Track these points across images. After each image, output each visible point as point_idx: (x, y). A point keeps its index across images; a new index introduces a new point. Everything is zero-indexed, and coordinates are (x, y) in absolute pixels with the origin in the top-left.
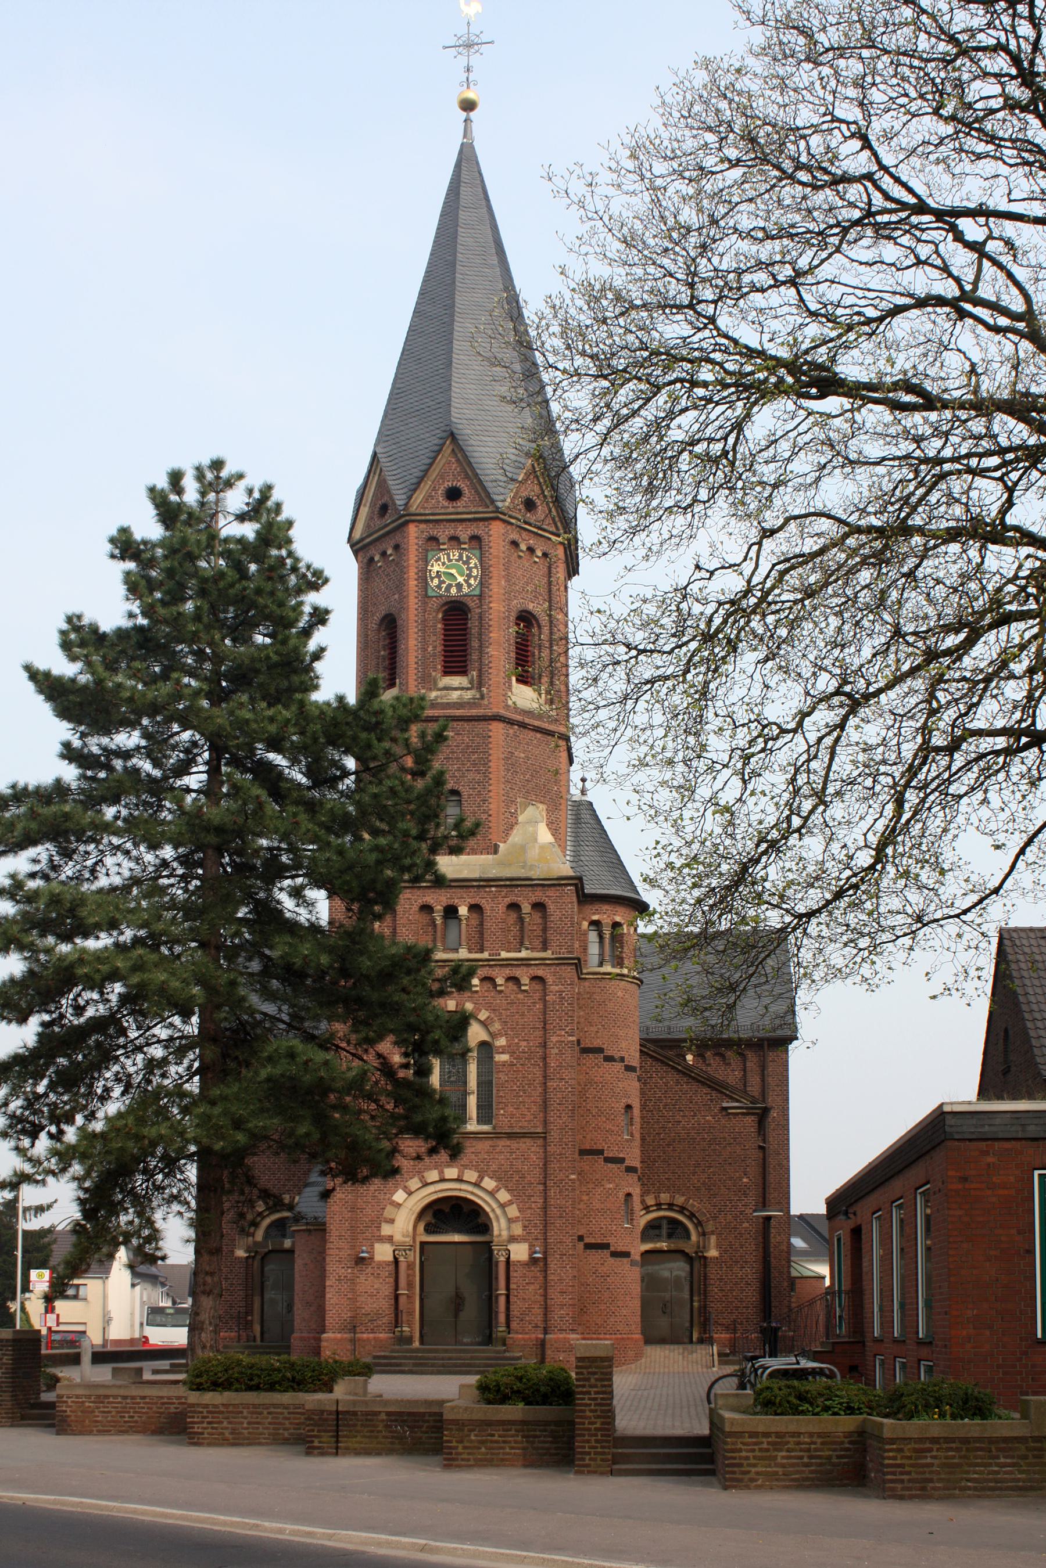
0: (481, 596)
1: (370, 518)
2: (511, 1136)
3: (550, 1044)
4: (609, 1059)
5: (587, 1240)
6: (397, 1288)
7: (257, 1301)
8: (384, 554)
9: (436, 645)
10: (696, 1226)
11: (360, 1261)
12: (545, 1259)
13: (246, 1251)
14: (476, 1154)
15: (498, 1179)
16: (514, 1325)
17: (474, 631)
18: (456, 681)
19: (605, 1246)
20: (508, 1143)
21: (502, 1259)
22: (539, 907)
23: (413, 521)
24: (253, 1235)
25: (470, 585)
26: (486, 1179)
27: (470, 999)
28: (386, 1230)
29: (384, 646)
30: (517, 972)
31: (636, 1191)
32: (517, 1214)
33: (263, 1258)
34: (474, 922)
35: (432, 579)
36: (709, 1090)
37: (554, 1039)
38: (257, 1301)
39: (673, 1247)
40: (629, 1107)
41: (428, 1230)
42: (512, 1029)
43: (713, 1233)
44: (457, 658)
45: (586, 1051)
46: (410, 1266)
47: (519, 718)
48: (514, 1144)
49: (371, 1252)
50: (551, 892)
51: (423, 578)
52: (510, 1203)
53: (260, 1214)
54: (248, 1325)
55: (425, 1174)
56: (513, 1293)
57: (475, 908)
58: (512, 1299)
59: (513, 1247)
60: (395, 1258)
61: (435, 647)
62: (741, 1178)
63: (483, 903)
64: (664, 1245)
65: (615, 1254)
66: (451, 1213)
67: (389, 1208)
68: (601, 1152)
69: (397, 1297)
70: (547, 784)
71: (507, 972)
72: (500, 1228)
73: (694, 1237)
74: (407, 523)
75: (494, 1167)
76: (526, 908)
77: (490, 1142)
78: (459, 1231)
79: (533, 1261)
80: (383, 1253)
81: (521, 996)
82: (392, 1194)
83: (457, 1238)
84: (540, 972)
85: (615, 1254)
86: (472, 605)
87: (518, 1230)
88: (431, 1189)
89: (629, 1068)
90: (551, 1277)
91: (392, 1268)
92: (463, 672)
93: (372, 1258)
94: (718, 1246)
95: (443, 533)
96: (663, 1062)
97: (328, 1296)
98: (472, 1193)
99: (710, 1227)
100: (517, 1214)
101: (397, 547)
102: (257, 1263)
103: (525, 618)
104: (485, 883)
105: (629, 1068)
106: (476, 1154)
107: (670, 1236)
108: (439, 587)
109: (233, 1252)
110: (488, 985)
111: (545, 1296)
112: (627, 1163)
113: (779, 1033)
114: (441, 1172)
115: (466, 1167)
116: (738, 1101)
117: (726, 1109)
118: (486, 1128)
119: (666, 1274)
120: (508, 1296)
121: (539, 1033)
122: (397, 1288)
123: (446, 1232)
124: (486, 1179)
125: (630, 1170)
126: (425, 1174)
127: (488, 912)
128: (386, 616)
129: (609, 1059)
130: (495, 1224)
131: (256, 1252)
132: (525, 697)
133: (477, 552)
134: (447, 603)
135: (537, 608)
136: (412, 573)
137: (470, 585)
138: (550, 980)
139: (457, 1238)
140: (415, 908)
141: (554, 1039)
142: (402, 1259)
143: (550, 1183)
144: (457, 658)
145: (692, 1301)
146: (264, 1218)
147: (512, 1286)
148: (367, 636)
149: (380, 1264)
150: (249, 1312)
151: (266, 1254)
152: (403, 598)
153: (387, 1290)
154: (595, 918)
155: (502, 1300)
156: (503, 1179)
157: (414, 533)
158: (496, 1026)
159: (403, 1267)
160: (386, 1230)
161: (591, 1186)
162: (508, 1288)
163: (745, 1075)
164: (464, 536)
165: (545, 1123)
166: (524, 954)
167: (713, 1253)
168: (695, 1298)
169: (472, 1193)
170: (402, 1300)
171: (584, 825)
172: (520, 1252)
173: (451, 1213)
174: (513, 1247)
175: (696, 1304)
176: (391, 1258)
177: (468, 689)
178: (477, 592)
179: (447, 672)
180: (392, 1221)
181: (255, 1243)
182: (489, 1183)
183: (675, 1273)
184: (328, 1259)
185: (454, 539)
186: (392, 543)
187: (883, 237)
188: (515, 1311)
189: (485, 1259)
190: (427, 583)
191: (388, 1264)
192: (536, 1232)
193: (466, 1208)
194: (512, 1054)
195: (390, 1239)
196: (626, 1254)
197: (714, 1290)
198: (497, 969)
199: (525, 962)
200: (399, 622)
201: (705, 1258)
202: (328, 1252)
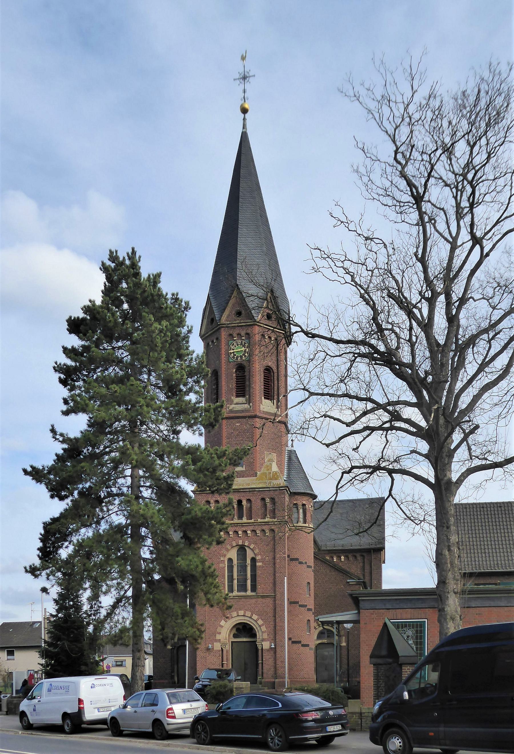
1: (207, 325)
2: (263, 597)
4: (301, 563)
5: (293, 640)
7: (176, 667)
8: (213, 342)
9: (233, 385)
12: (275, 648)
15: (258, 615)
16: (264, 675)
18: (241, 400)
19: (299, 642)
20: (262, 600)
23: (223, 327)
25: (245, 356)
28: (218, 637)
30: (264, 528)
31: (312, 618)
36: (342, 574)
37: (278, 556)
38: (176, 667)
39: (329, 642)
40: (309, 583)
41: (235, 636)
44: (242, 389)
45: (292, 560)
46: (227, 651)
47: (264, 416)
48: (264, 600)
49: (213, 647)
52: (263, 625)
54: (172, 677)
56: (264, 662)
61: (232, 385)
63: (251, 498)
64: (325, 641)
65: (304, 646)
68: (298, 603)
70: (278, 444)
72: (259, 635)
74: (219, 329)
75: (257, 610)
77: (255, 600)
78: (245, 637)
80: (217, 646)
83: (245, 640)
85: (304, 646)
87: (265, 636)
88: (234, 619)
89: (309, 567)
92: (244, 396)
96: (325, 562)
101: (217, 339)
102: (175, 651)
104: (252, 490)
105: (309, 567)
107: (328, 637)
110: (253, 533)
111: (275, 663)
112: (308, 607)
113: (378, 546)
114: (238, 613)
115: (246, 610)
116: (353, 579)
117: (349, 582)
118: (254, 594)
119: (326, 653)
120: (262, 663)
121: (272, 553)
123: (241, 637)
125: (309, 610)
127: (253, 502)
128: (214, 370)
129: (301, 563)
130: (257, 634)
131: (175, 647)
132: (267, 406)
135: (272, 364)
136: (223, 351)
137: (245, 356)
139: (245, 640)
142: (224, 649)
143: (277, 616)
144: (242, 389)
147: (264, 659)
150: (173, 671)
152: (220, 362)
154: (295, 502)
156: (260, 615)
158: (257, 551)
159: (225, 652)
160: (218, 637)
161: (294, 617)
163: (364, 565)
164: (243, 333)
165: (275, 591)
166: (267, 520)
171: (293, 461)
172: (266, 645)
173: (244, 629)
177: (245, 404)
179: (237, 396)
181: (175, 643)
182: (255, 617)
183: (330, 653)
186: (215, 337)
187: (278, 321)
188: (265, 671)
189: (254, 650)
190: (229, 356)
191: (219, 651)
192: (272, 637)
193: (248, 627)
194: (263, 562)
196: (307, 645)
199: (267, 523)
200: (219, 374)
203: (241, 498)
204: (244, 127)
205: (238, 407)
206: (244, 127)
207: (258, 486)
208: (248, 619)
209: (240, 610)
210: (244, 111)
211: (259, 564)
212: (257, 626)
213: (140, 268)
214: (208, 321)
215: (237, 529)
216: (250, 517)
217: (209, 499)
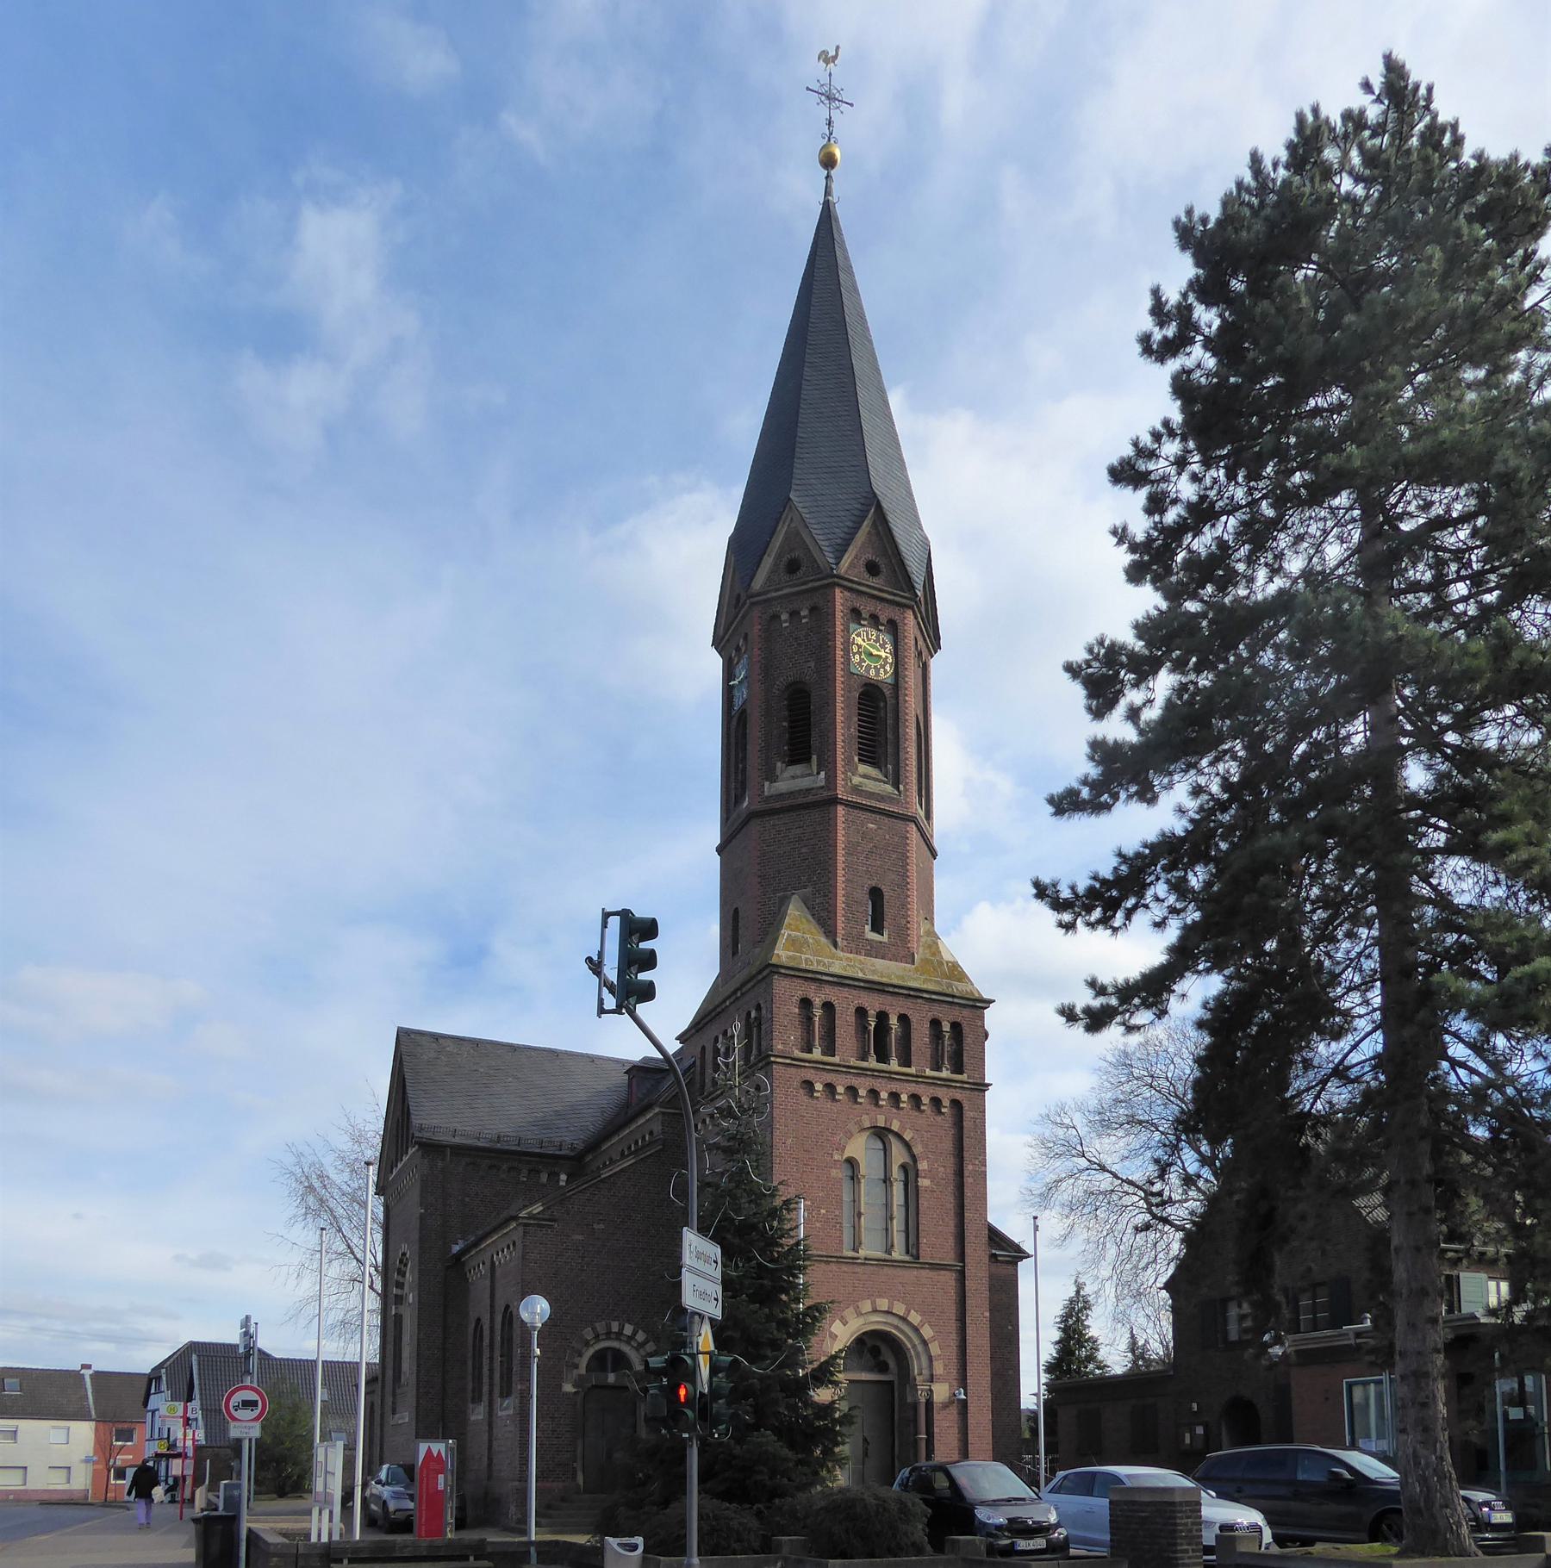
3: (966, 1173)
15: (923, 1314)
18: (797, 769)
24: (576, 1366)
37: (970, 1167)
48: (931, 1274)
57: (903, 1019)
81: (939, 1118)
98: (896, 1327)
155: (923, 1445)
172: (941, 1392)
203: (887, 1009)
204: (828, 192)
205: (871, 786)
206: (828, 192)
207: (924, 987)
208: (896, 1321)
209: (880, 1296)
210: (828, 162)
211: (924, 1182)
212: (917, 1341)
213: (1170, 333)
214: (776, 564)
215: (855, 1082)
216: (906, 1061)
217: (811, 996)
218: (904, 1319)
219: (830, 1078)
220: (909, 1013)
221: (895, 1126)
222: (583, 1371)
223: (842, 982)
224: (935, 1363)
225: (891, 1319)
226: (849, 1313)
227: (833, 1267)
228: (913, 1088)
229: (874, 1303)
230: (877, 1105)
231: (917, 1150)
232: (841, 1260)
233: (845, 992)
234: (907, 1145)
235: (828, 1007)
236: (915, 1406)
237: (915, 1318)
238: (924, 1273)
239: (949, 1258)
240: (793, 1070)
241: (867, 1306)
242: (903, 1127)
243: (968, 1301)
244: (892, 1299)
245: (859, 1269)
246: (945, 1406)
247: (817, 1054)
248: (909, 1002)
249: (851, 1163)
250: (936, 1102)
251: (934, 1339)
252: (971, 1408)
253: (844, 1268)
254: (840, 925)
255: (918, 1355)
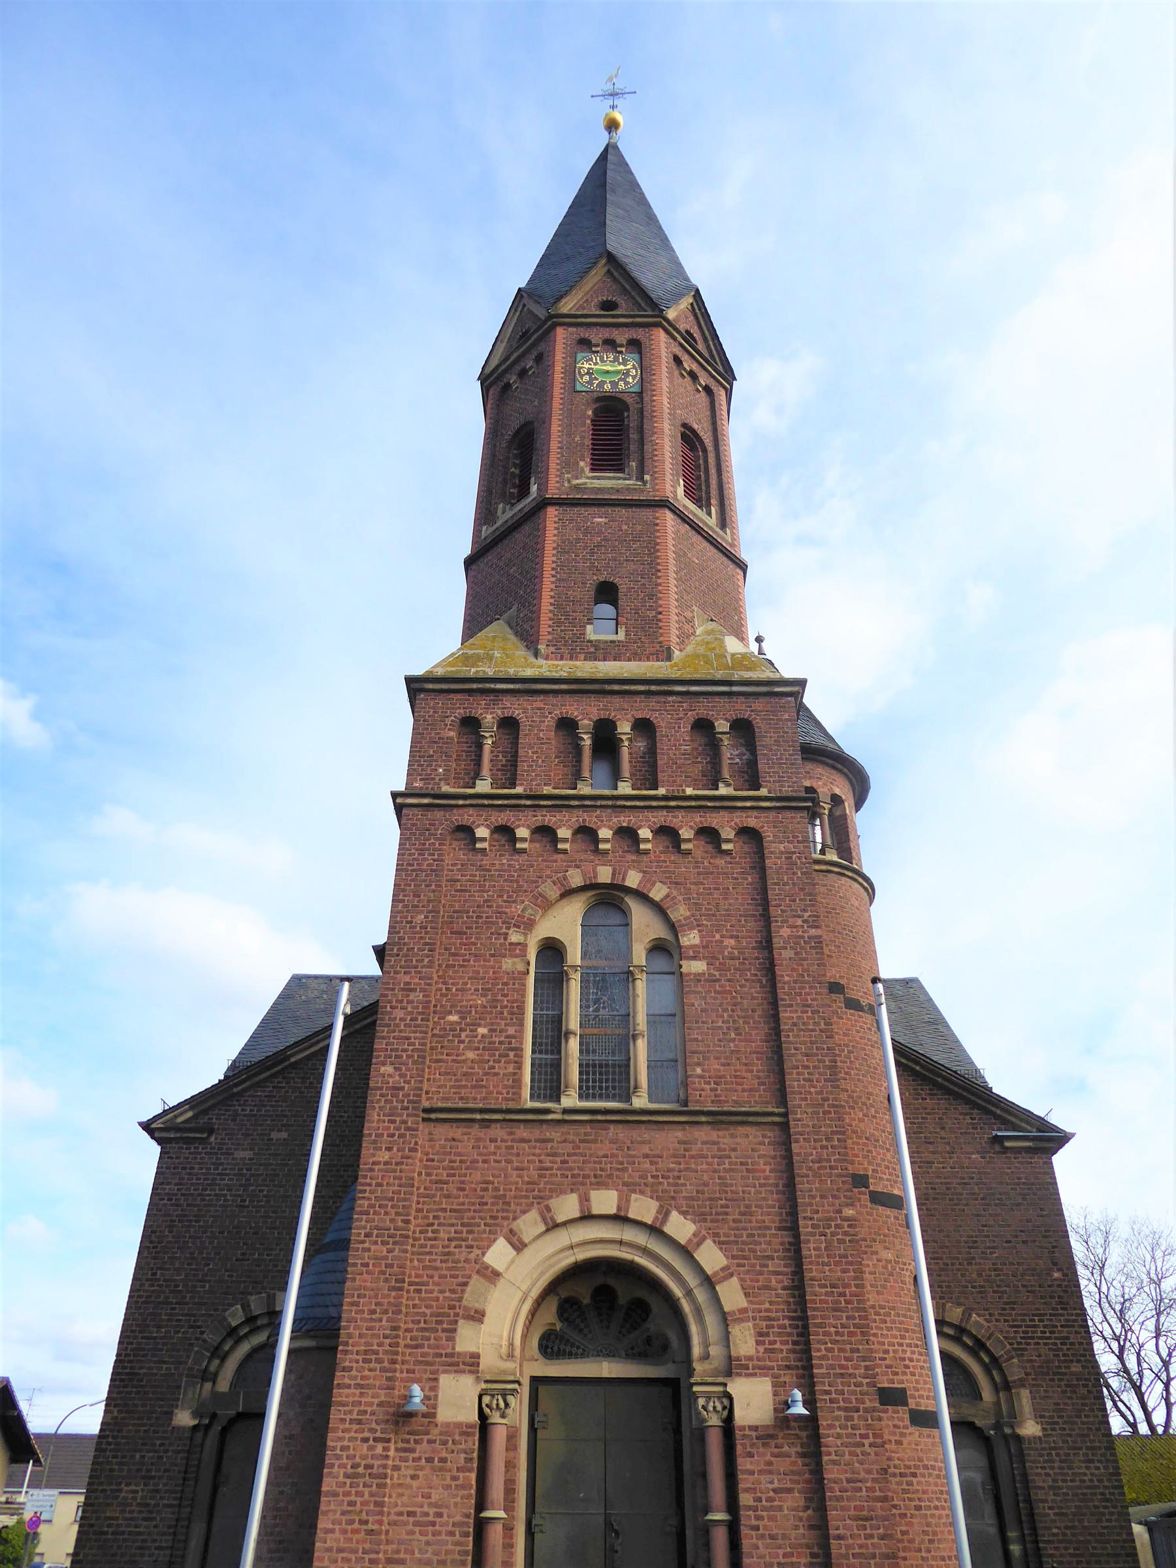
0: (640, 394)
3: (777, 942)
6: (481, 1505)
9: (584, 435)
10: (987, 1369)
11: (402, 1417)
13: (196, 1414)
14: (653, 1158)
17: (633, 424)
20: (714, 1135)
21: (714, 1420)
22: (743, 728)
24: (214, 1379)
25: (626, 383)
26: (675, 1216)
27: (636, 865)
28: (468, 1339)
29: (516, 457)
32: (743, 1303)
33: (224, 1430)
34: (641, 745)
35: (582, 376)
37: (785, 932)
42: (710, 916)
43: (1022, 1384)
48: (724, 1138)
50: (759, 704)
51: (571, 373)
53: (233, 1331)
55: (553, 1203)
56: (747, 1518)
57: (644, 727)
58: (748, 1541)
59: (738, 1388)
60: (482, 1416)
61: (582, 438)
62: (1049, 1273)
66: (602, 1302)
67: (476, 1282)
69: (481, 1527)
71: (698, 819)
73: (987, 1394)
74: (555, 325)
75: (689, 1189)
76: (722, 726)
78: (610, 1353)
79: (783, 1420)
80: (457, 1399)
81: (720, 862)
82: (484, 1250)
83: (607, 1369)
84: (752, 822)
86: (629, 400)
88: (563, 1238)
90: (831, 1473)
91: (474, 1443)
93: (431, 1415)
94: (1039, 1416)
95: (596, 336)
97: (323, 1523)
98: (645, 1251)
99: (1014, 1370)
100: (743, 1303)
103: (689, 437)
106: (653, 1158)
108: (590, 382)
109: (170, 1415)
110: (664, 842)
114: (585, 1200)
117: (998, 1140)
120: (733, 1527)
122: (481, 1505)
124: (675, 1216)
126: (553, 1203)
131: (214, 1416)
133: (636, 356)
134: (598, 399)
137: (626, 383)
138: (768, 834)
139: (607, 1369)
140: (550, 722)
141: (785, 932)
142: (495, 1418)
145: (1005, 1541)
146: (239, 1341)
147: (745, 1499)
148: (494, 456)
149: (450, 1429)
151: (232, 1422)
153: (460, 1507)
155: (720, 1538)
157: (562, 336)
160: (468, 1339)
162: (732, 1505)
167: (1030, 1429)
168: (1012, 1534)
169: (645, 1251)
170: (495, 1534)
172: (753, 1400)
174: (738, 1388)
175: (1015, 1549)
176: (474, 1417)
178: (636, 389)
180: (478, 1316)
181: (215, 1395)
184: (335, 1414)
185: (611, 344)
190: (574, 380)
191: (464, 1430)
192: (784, 1348)
194: (711, 960)
195: (471, 1363)
197: (1046, 1511)
198: (680, 814)
201: (1018, 1439)
202: (339, 1395)
212: (692, 1281)
217: (478, 712)
218: (655, 1230)
219: (502, 818)
220: (654, 717)
221: (633, 880)
222: (223, 1385)
223: (531, 688)
224: (735, 1330)
225: (630, 1234)
226: (529, 1224)
227: (498, 1132)
228: (661, 818)
229: (585, 1200)
230: (597, 851)
231: (679, 913)
232: (513, 1116)
233: (539, 702)
234: (659, 909)
235: (509, 725)
236: (701, 1434)
237: (680, 1227)
238: (702, 1134)
239: (758, 1100)
240: (439, 814)
241: (567, 1206)
242: (648, 880)
243: (802, 1186)
244: (628, 1189)
245: (555, 1134)
246: (765, 1435)
247: (483, 786)
248: (653, 702)
249: (552, 950)
250: (709, 834)
251: (726, 1273)
252: (831, 1439)
253: (522, 1132)
254: (544, 629)
255: (698, 1311)
